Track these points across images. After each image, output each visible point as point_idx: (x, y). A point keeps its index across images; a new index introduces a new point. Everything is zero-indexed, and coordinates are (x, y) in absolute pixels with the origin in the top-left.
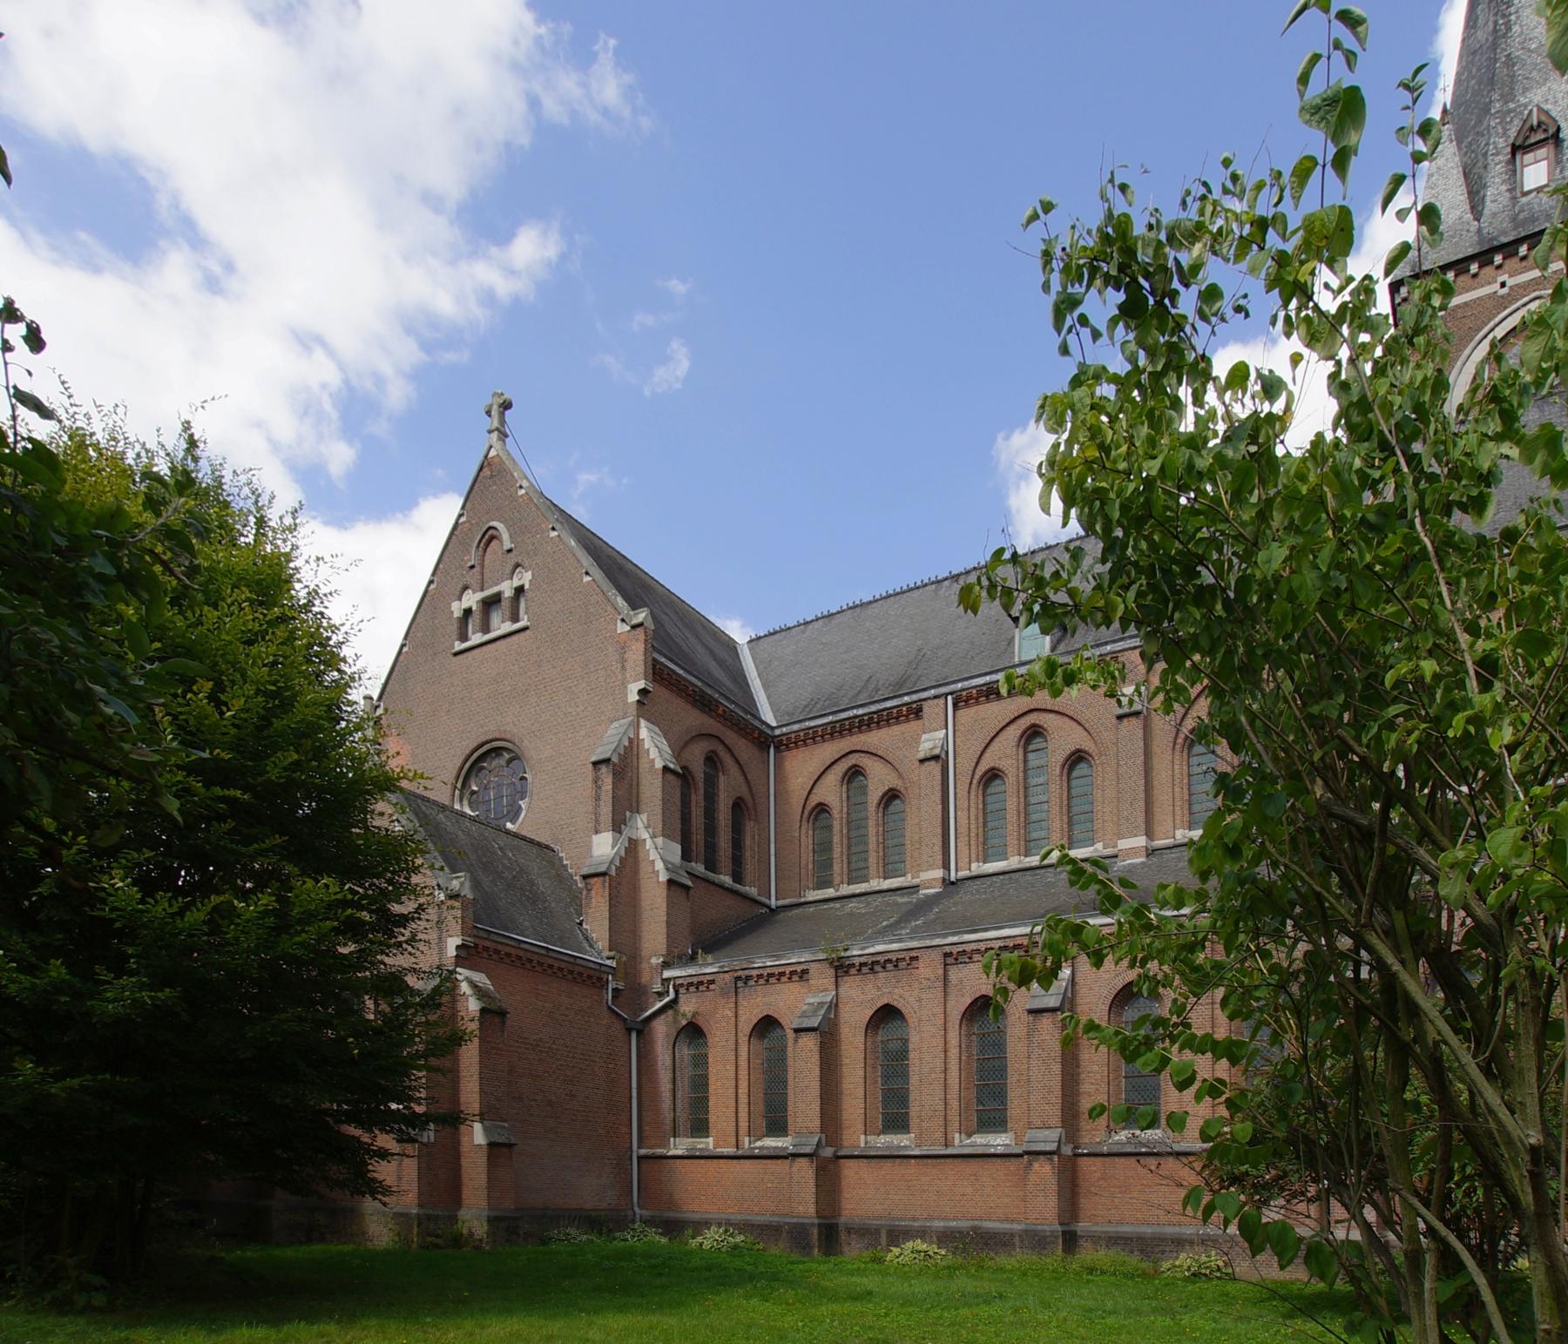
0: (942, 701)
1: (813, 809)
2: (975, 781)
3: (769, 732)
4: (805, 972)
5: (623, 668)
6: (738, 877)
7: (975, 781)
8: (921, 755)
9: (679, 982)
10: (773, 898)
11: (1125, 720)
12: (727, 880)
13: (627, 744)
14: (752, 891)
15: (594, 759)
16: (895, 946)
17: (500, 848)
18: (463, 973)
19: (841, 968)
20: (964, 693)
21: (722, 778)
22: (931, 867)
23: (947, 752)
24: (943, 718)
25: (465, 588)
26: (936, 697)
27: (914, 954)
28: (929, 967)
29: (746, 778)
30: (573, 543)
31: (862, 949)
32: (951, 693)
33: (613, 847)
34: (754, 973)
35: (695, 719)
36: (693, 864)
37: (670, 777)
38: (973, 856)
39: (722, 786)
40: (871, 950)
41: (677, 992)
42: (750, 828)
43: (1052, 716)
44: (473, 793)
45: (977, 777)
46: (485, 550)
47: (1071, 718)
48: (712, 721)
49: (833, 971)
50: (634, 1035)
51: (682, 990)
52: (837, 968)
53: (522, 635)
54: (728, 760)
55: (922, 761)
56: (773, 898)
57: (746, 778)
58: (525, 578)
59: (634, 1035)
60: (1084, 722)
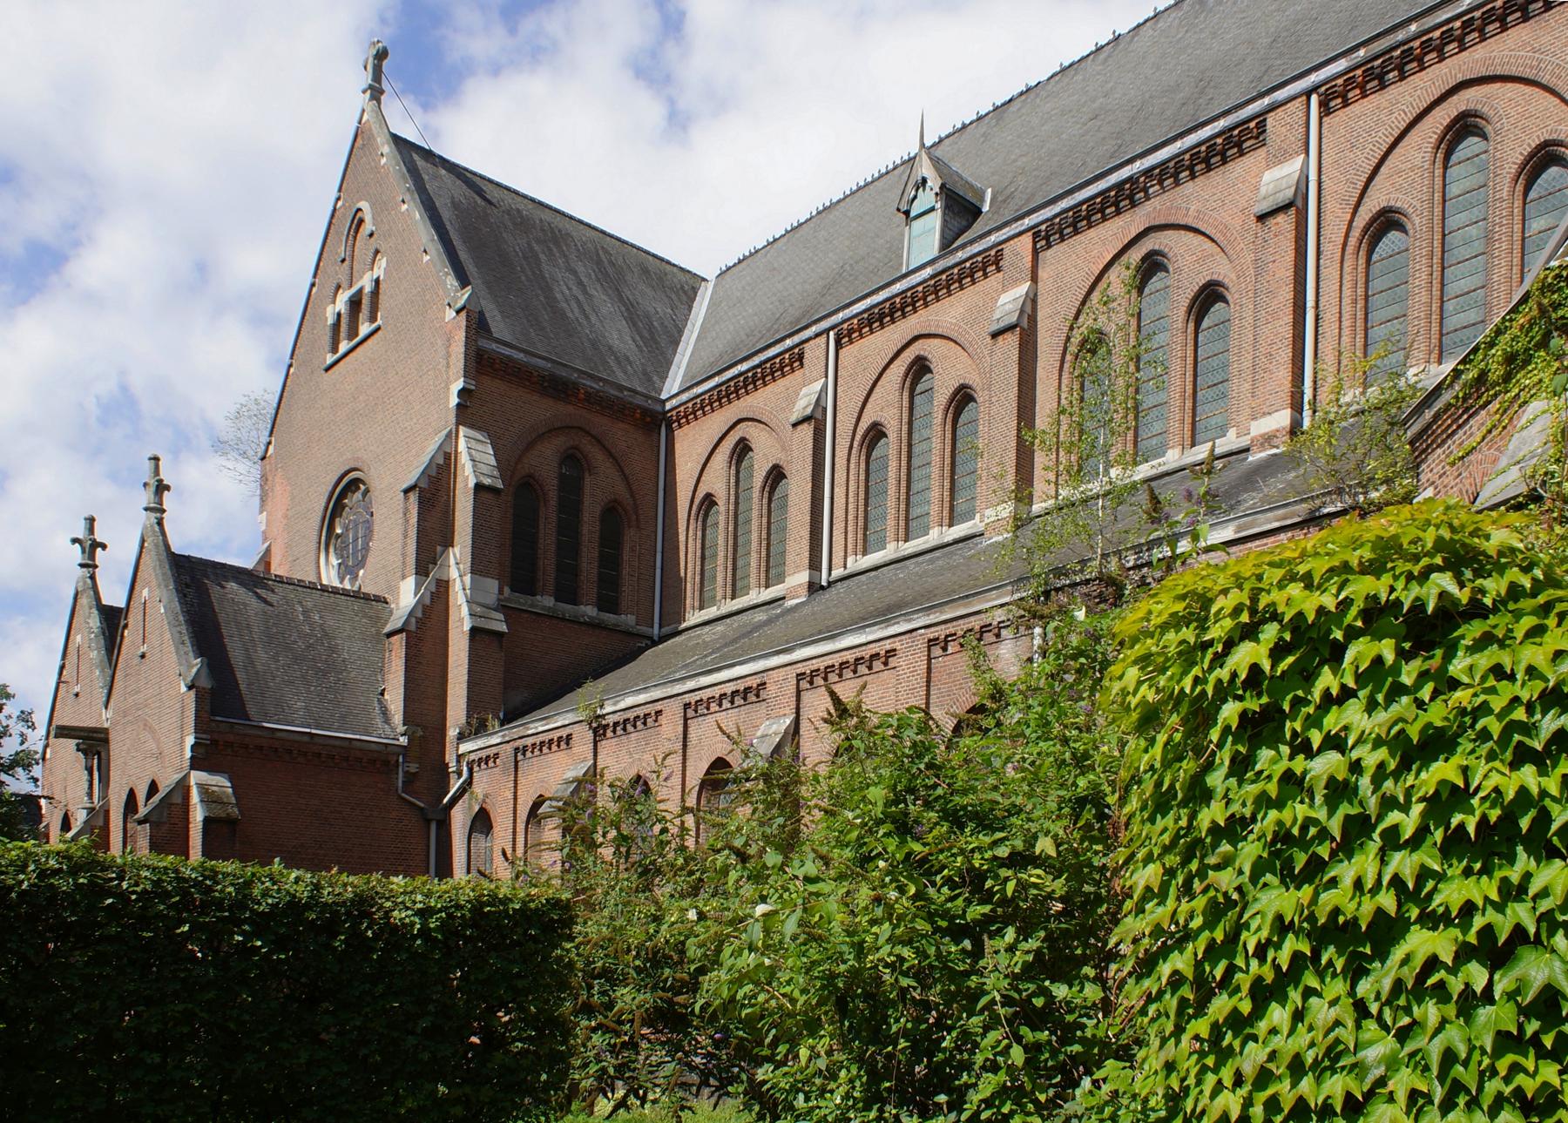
0: (823, 339)
1: (702, 503)
2: (856, 444)
3: (658, 408)
4: (569, 737)
5: (448, 366)
6: (609, 603)
7: (856, 444)
8: (794, 418)
9: (473, 757)
10: (656, 626)
11: (1000, 338)
12: (590, 611)
13: (441, 461)
14: (628, 620)
15: (405, 486)
16: (642, 698)
17: (1518, 381)
18: (196, 777)
19: (600, 731)
20: (845, 326)
21: (588, 480)
22: (797, 570)
23: (825, 409)
24: (823, 363)
25: (338, 287)
26: (817, 335)
27: (658, 706)
28: (670, 725)
29: (621, 470)
30: (418, 216)
31: (615, 704)
32: (832, 328)
33: (416, 595)
34: (529, 741)
35: (543, 410)
36: (539, 597)
37: (485, 496)
38: (850, 546)
39: (587, 490)
40: (622, 705)
41: (471, 771)
42: (630, 536)
43: (936, 341)
44: (338, 536)
45: (858, 438)
46: (355, 238)
47: (956, 342)
48: (571, 409)
49: (590, 734)
50: (433, 827)
51: (476, 768)
52: (595, 731)
53: (376, 336)
54: (598, 457)
55: (795, 425)
56: (656, 626)
57: (621, 470)
58: (379, 270)
59: (433, 827)
60: (967, 345)
